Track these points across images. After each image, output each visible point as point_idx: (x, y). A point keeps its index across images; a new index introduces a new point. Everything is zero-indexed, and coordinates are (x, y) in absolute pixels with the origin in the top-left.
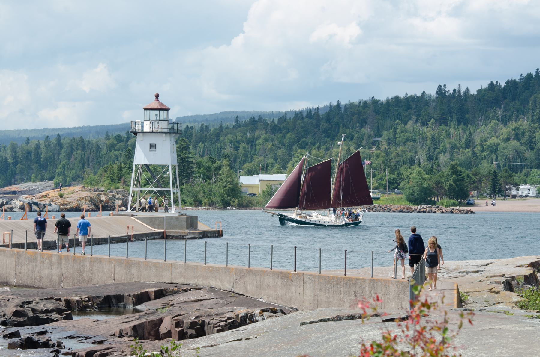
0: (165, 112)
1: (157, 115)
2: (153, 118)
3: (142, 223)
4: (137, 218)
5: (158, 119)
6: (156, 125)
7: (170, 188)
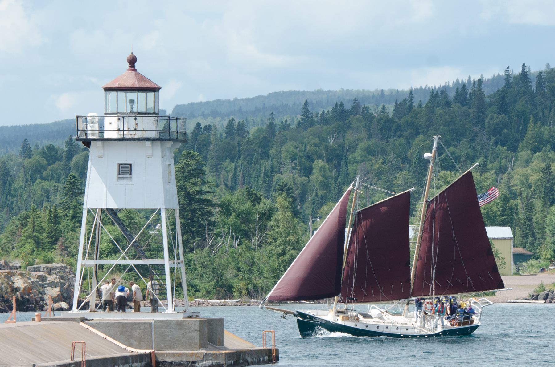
0: (151, 95)
1: (132, 102)
2: (125, 108)
3: (104, 336)
4: (93, 326)
5: (135, 110)
6: (130, 123)
7: (162, 258)
